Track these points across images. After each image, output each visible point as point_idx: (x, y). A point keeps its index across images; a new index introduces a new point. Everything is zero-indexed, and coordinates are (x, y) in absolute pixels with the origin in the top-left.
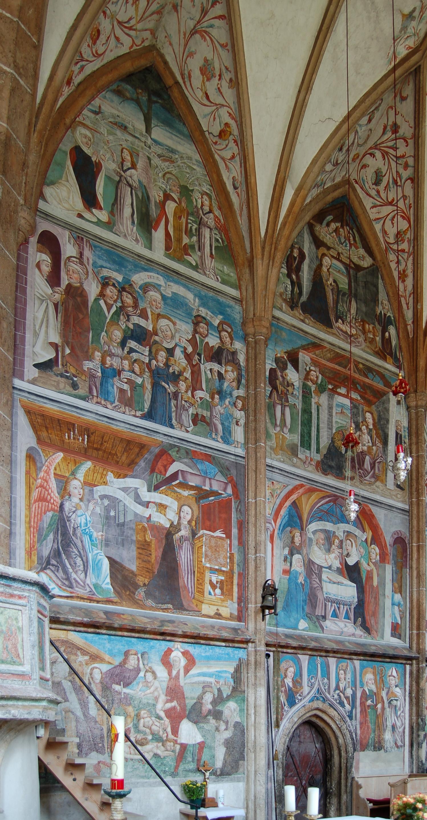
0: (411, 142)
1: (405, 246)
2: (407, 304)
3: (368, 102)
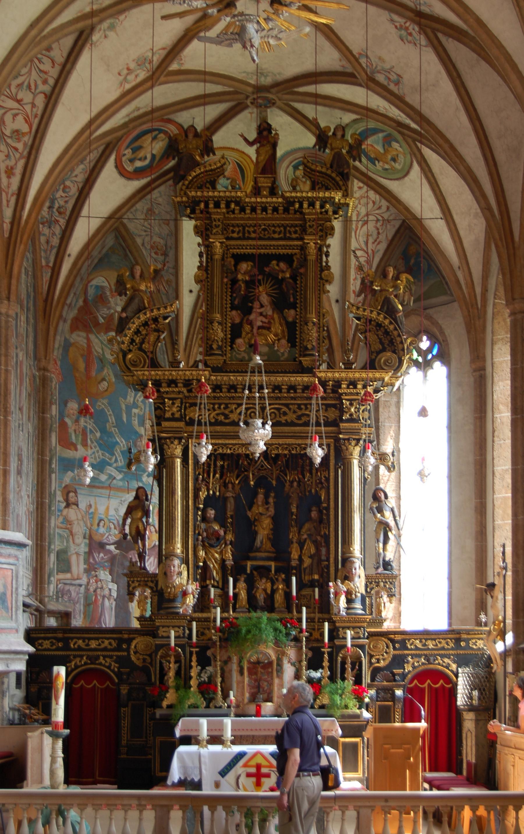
0: (58, 68)
1: (20, 146)
2: (8, 201)
3: (99, 236)
